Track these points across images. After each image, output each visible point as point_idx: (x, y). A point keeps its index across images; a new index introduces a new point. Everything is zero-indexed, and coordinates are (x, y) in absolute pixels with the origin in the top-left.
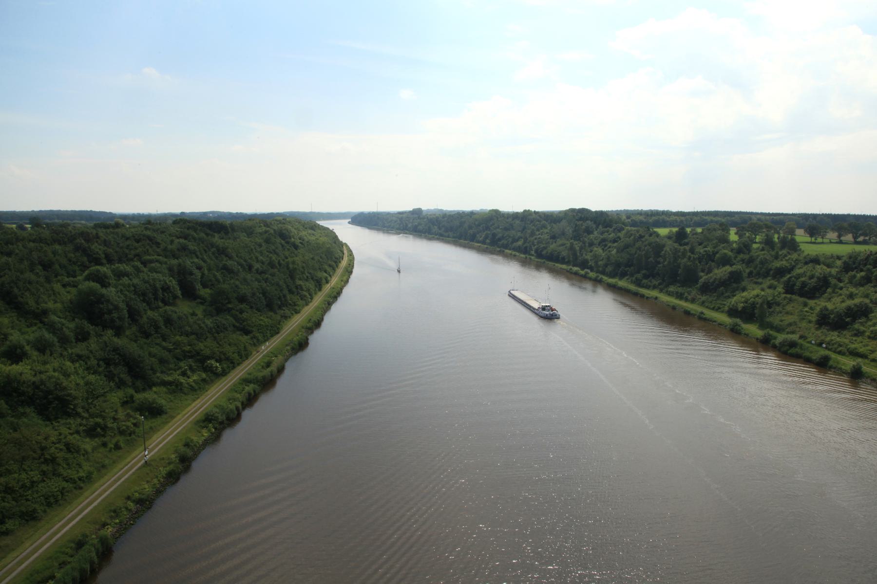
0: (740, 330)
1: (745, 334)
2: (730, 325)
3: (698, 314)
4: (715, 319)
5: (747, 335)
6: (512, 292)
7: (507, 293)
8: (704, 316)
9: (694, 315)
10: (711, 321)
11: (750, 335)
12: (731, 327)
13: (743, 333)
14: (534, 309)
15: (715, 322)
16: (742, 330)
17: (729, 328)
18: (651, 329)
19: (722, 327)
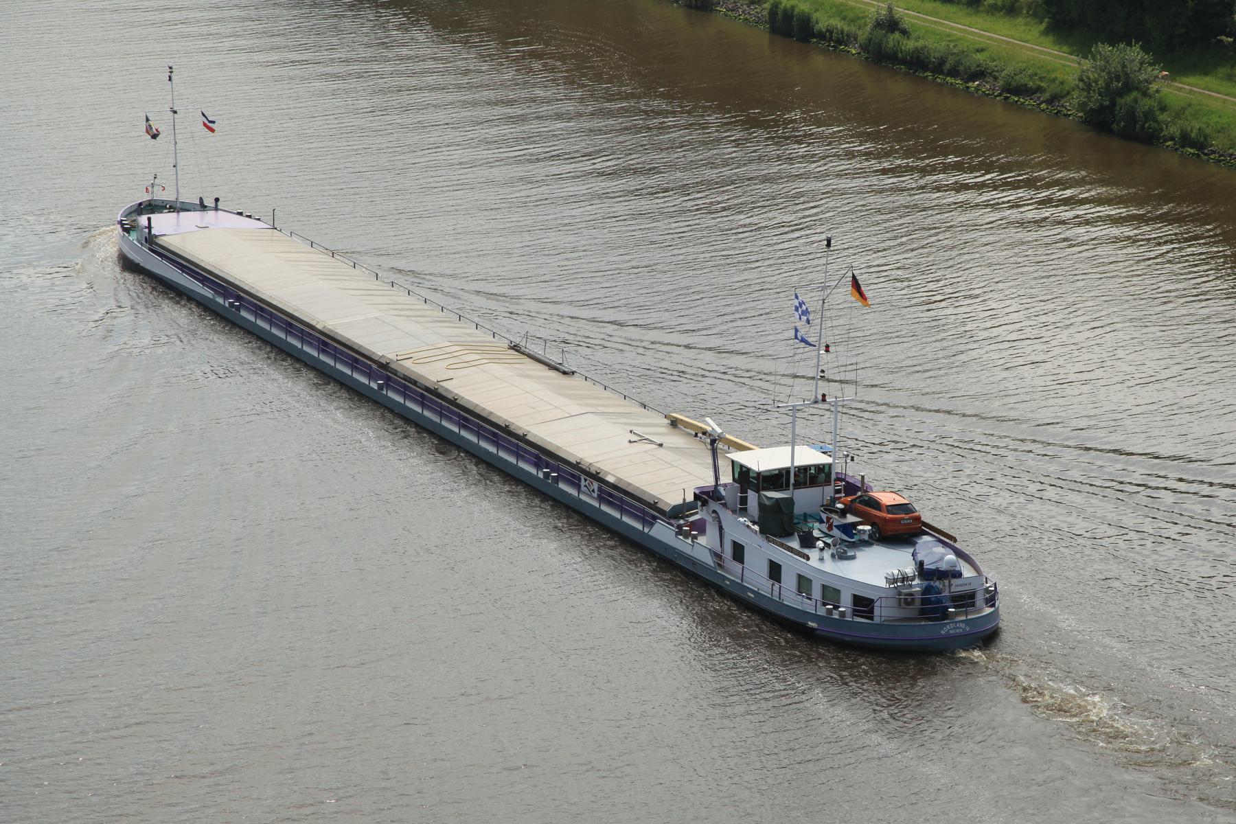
0: (1149, 115)
1: (1186, 139)
2: (1088, 87)
3: (863, 35)
4: (980, 57)
5: (1196, 144)
6: (162, 224)
7: (110, 242)
8: (910, 45)
9: (835, 41)
10: (954, 73)
11: (1217, 143)
12: (1095, 100)
13: (1174, 130)
14: (648, 509)
15: (980, 74)
16: (1163, 117)
17: (1082, 106)
18: (203, 37)
19: (1029, 102)
